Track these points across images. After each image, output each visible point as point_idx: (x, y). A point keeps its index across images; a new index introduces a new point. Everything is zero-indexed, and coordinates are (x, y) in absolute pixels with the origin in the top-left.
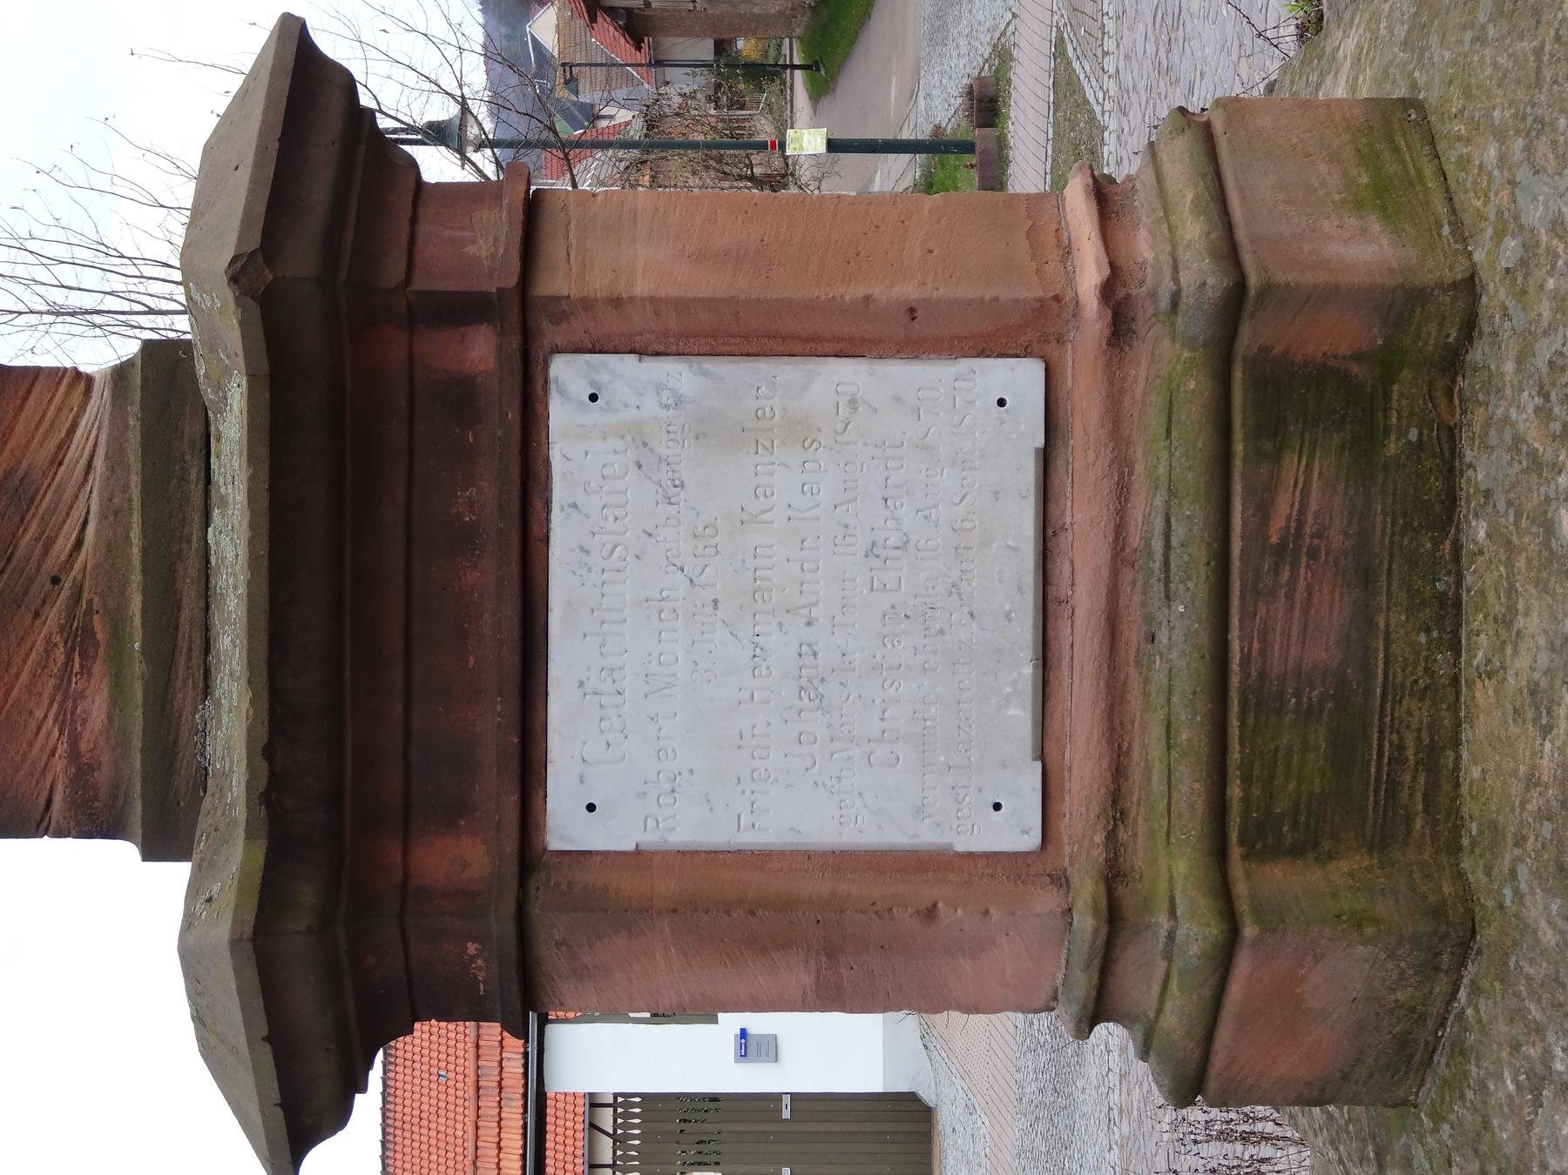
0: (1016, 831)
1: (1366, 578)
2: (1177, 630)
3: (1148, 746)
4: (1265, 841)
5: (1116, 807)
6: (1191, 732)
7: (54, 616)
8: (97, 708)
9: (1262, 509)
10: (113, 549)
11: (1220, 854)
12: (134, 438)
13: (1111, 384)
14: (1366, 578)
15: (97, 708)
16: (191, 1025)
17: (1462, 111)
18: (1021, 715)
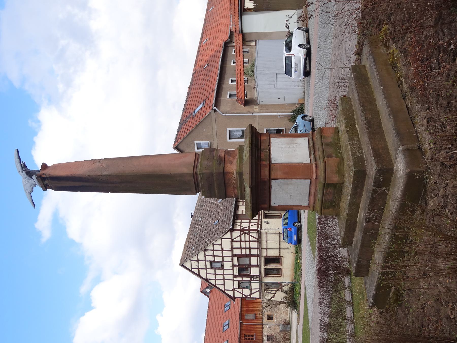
0: (307, 204)
1: (334, 195)
2: (319, 197)
3: (317, 200)
4: (324, 208)
5: (314, 203)
6: (320, 202)
7: (232, 186)
8: (236, 191)
9: (326, 191)
10: (237, 182)
11: (321, 209)
12: (238, 177)
13: (295, 278)
14: (334, 195)
15: (236, 191)
16: (183, 248)
17: (433, 220)
18: (307, 199)
